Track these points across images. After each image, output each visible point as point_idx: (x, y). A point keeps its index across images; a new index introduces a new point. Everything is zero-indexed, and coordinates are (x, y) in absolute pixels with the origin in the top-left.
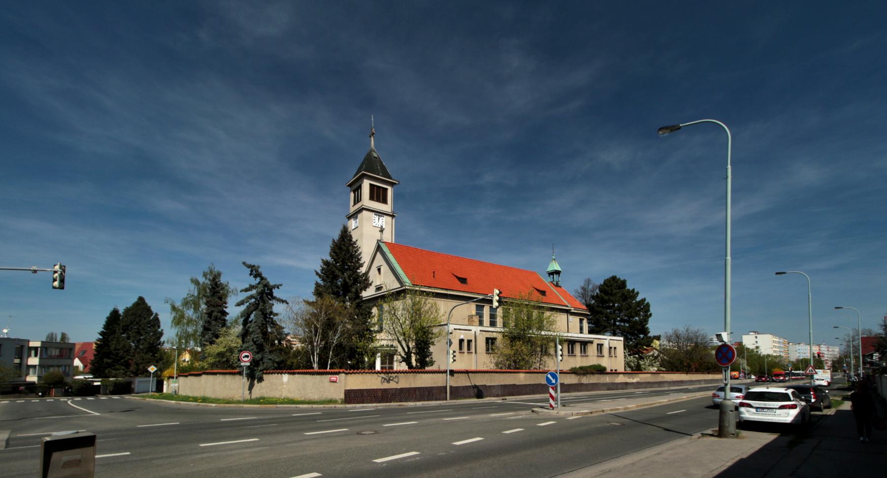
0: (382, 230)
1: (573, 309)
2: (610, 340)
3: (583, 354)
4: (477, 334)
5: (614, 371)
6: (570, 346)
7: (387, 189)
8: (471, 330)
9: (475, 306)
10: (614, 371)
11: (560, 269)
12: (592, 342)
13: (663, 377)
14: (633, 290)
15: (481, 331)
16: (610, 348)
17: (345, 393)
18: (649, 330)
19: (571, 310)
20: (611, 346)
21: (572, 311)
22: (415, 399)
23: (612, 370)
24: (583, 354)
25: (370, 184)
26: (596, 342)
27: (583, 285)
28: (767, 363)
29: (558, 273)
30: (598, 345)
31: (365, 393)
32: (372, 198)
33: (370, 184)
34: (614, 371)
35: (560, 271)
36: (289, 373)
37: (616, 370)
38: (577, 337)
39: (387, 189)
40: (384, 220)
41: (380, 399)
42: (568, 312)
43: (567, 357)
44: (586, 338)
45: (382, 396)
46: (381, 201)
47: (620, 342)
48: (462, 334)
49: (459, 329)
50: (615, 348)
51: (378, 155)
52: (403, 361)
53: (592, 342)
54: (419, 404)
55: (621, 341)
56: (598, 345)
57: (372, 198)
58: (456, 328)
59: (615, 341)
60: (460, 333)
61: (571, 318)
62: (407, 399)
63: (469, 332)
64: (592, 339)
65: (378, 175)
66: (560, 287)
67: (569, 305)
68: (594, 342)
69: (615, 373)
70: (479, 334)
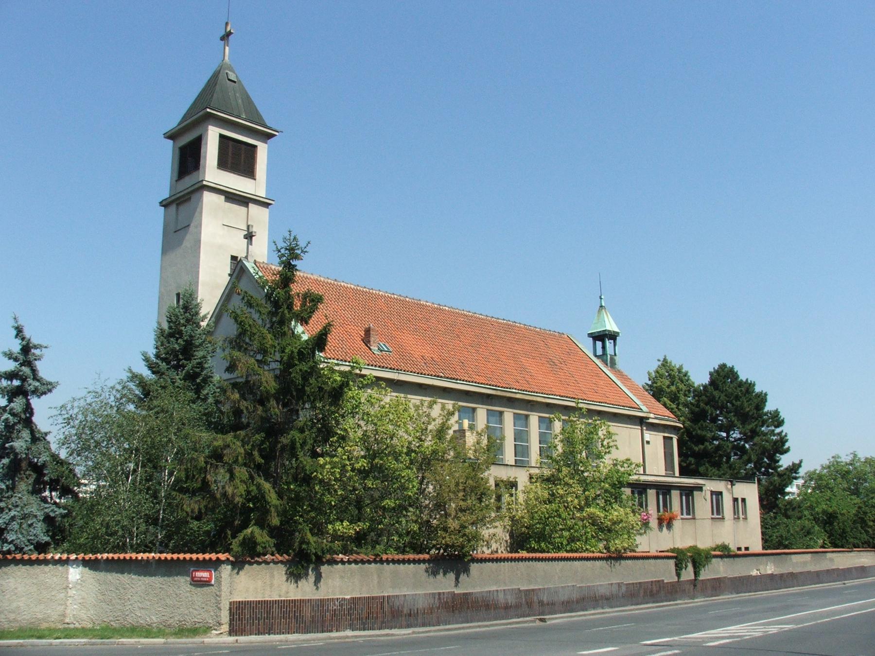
0: (249, 236)
1: (652, 416)
3: (715, 516)
5: (743, 549)
6: (661, 497)
7: (255, 147)
9: (537, 417)
10: (743, 549)
11: (616, 329)
13: (831, 560)
16: (735, 500)
17: (230, 609)
18: (791, 464)
19: (648, 418)
21: (651, 421)
22: (383, 622)
23: (739, 549)
24: (715, 516)
25: (222, 137)
28: (511, 552)
29: (613, 336)
30: (712, 493)
31: (275, 610)
32: (224, 164)
33: (222, 137)
34: (743, 551)
35: (618, 333)
36: (86, 563)
37: (747, 549)
39: (255, 147)
41: (308, 624)
42: (641, 421)
43: (710, 520)
45: (313, 617)
46: (229, 166)
50: (744, 500)
51: (237, 76)
52: (649, 527)
53: (700, 488)
54: (765, 593)
57: (224, 164)
61: (648, 436)
62: (364, 624)
65: (239, 117)
67: (644, 408)
68: (704, 488)
69: (745, 554)
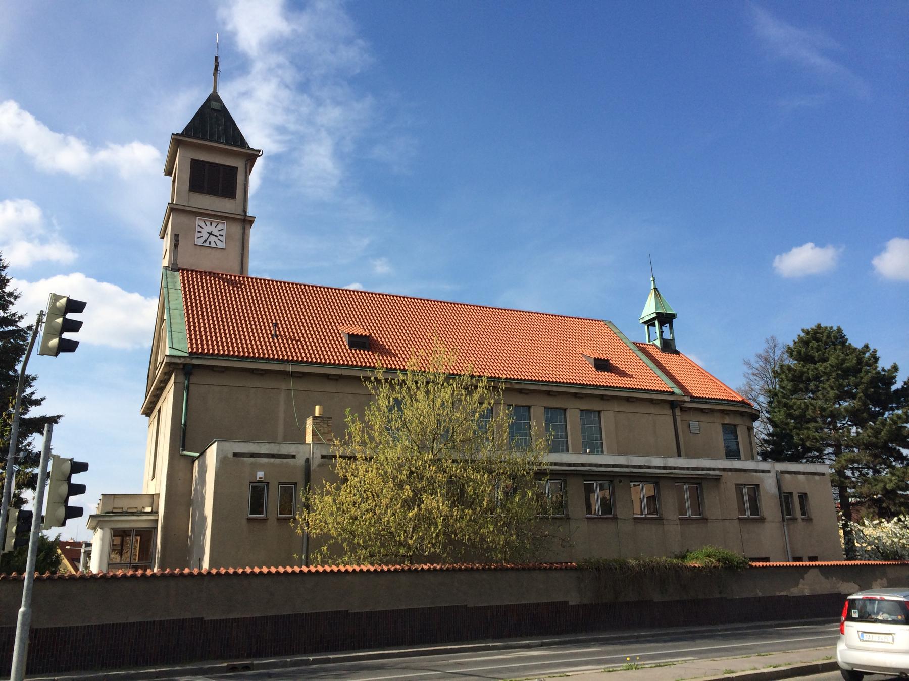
2: (782, 472)
4: (313, 466)
8: (294, 456)
12: (717, 479)
14: (866, 347)
15: (323, 457)
19: (685, 401)
20: (786, 489)
21: (686, 405)
26: (730, 482)
27: (761, 351)
38: (664, 468)
40: (198, 234)
44: (601, 465)
47: (817, 477)
48: (261, 467)
49: (252, 455)
50: (803, 497)
55: (823, 474)
56: (739, 488)
58: (324, 453)
59: (801, 477)
60: (252, 463)
63: (285, 460)
64: (717, 473)
66: (677, 353)
68: (723, 480)
70: (320, 465)
